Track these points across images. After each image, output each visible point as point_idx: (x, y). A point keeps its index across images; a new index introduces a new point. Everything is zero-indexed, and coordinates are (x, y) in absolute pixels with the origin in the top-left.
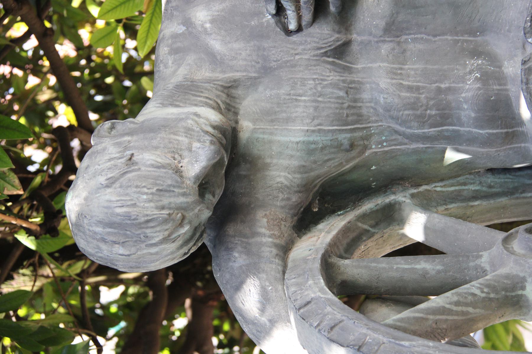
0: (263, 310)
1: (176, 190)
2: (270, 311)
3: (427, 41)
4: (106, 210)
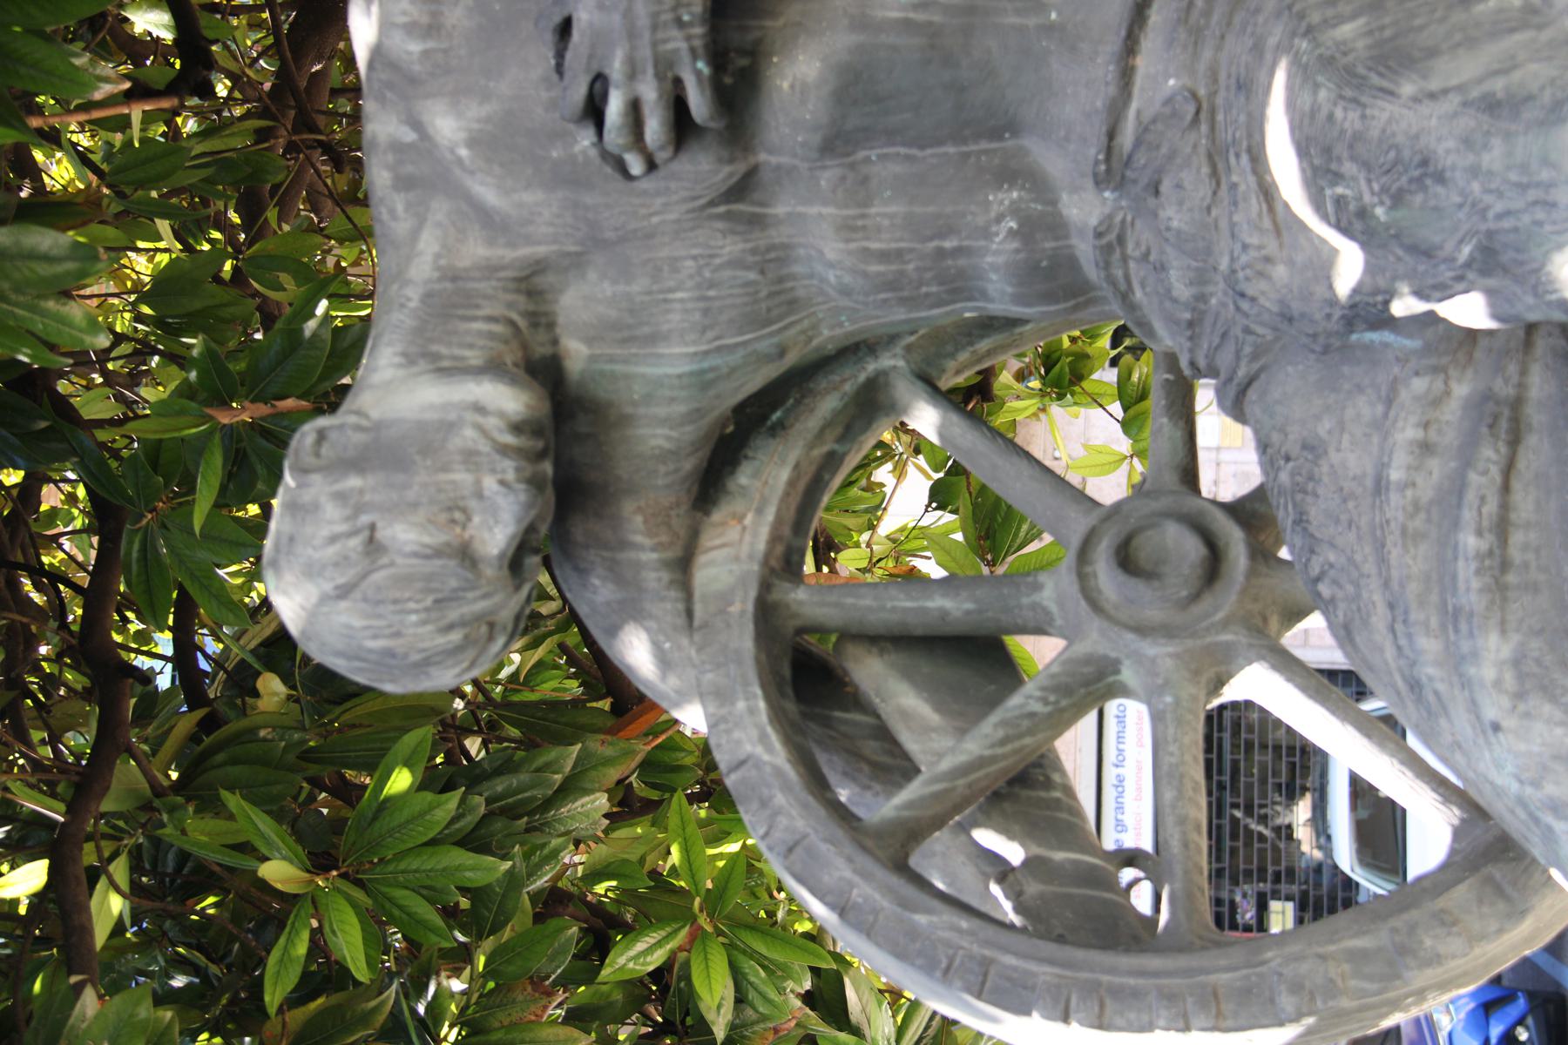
3: (908, 158)
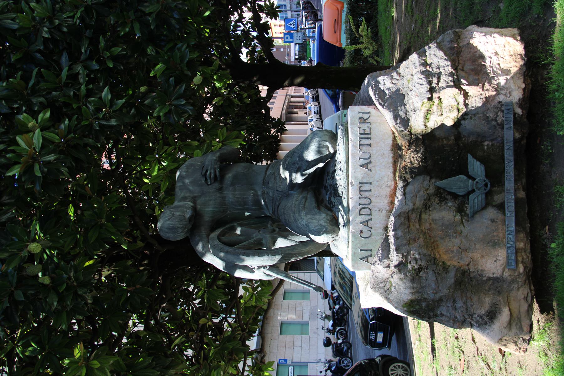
0: (203, 249)
2: (205, 250)
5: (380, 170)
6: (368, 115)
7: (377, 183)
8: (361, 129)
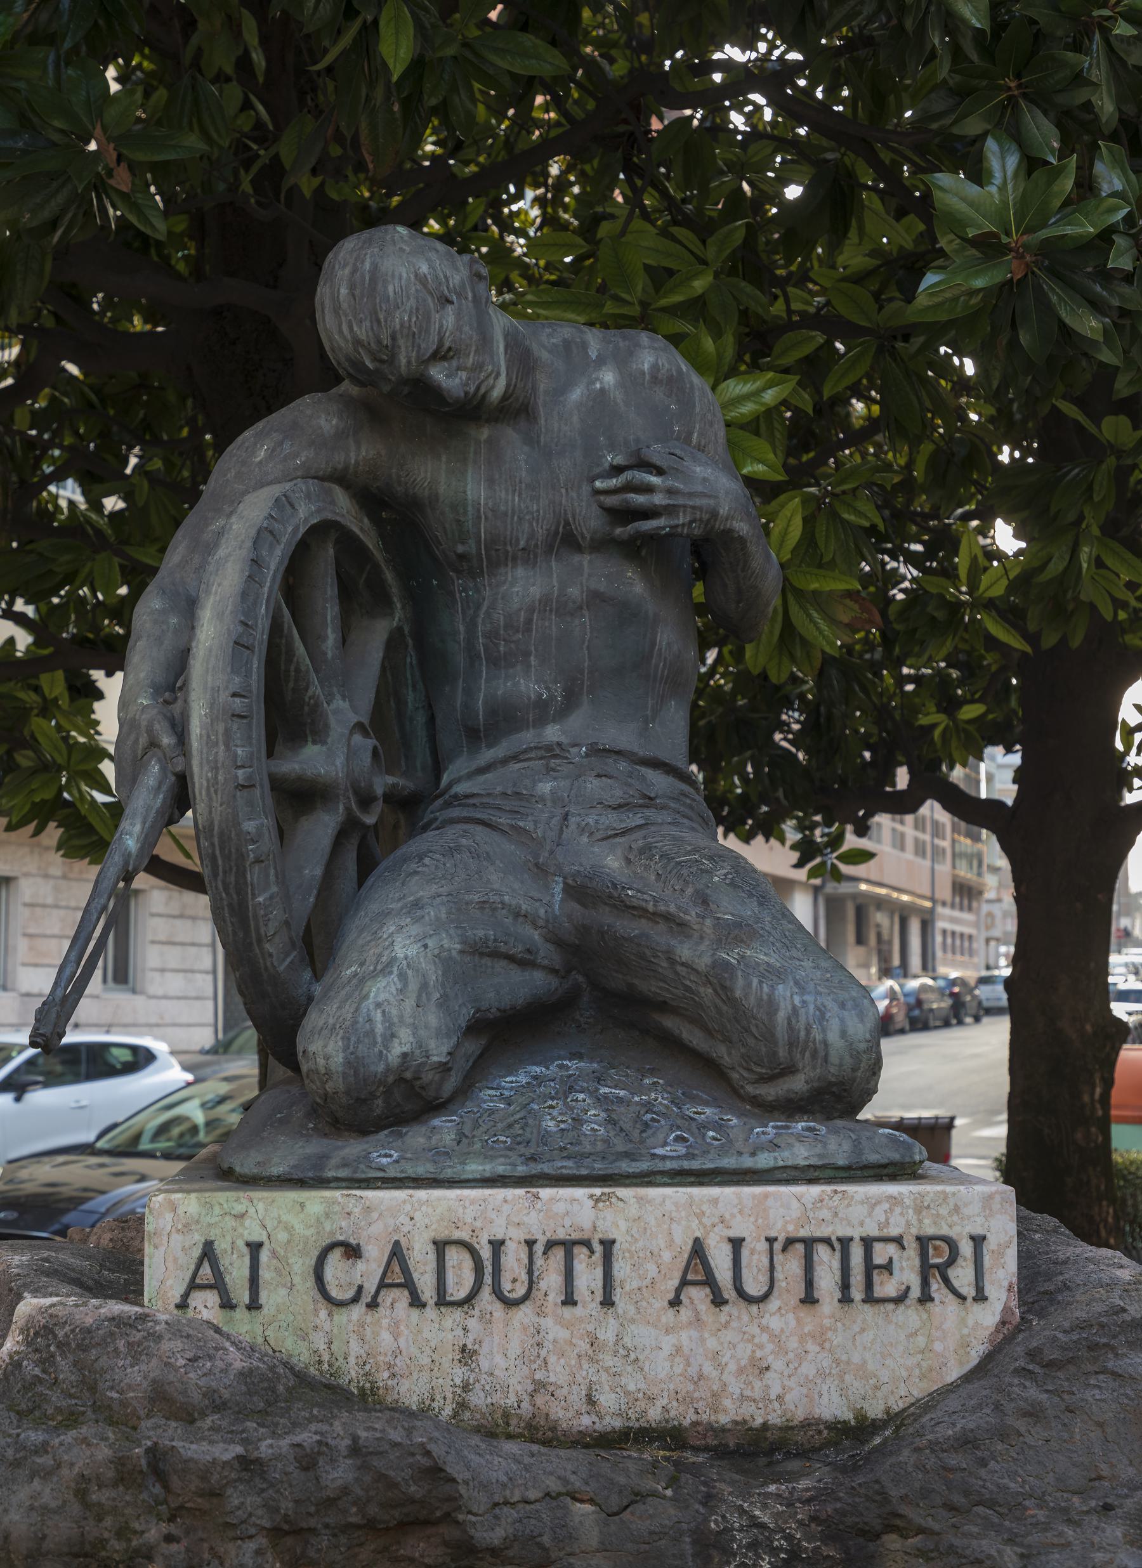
1: (414, 354)
4: (390, 273)
5: (678, 1350)
6: (969, 1291)
7: (607, 1334)
8: (892, 1249)
